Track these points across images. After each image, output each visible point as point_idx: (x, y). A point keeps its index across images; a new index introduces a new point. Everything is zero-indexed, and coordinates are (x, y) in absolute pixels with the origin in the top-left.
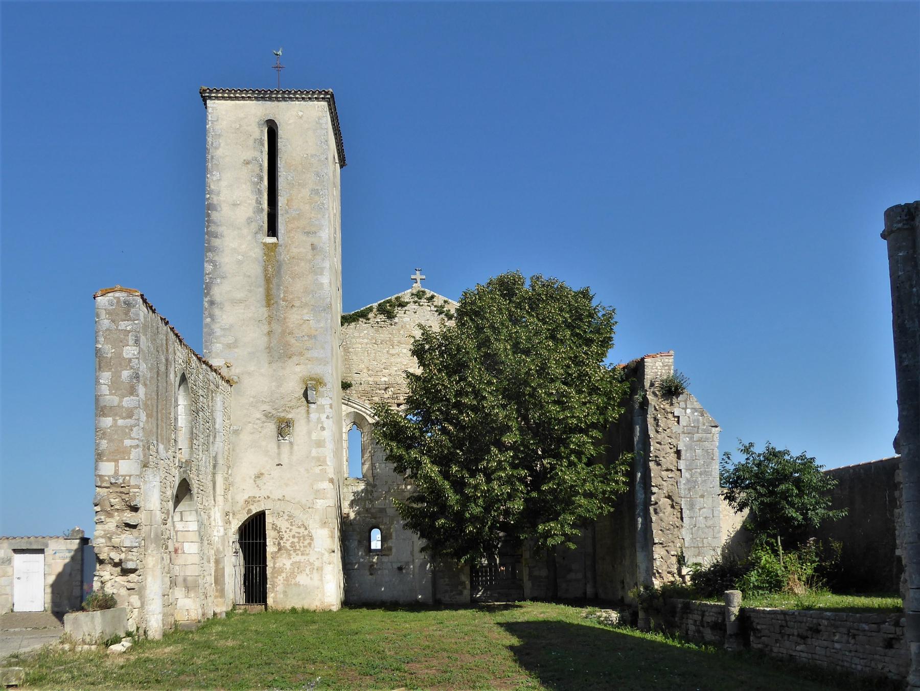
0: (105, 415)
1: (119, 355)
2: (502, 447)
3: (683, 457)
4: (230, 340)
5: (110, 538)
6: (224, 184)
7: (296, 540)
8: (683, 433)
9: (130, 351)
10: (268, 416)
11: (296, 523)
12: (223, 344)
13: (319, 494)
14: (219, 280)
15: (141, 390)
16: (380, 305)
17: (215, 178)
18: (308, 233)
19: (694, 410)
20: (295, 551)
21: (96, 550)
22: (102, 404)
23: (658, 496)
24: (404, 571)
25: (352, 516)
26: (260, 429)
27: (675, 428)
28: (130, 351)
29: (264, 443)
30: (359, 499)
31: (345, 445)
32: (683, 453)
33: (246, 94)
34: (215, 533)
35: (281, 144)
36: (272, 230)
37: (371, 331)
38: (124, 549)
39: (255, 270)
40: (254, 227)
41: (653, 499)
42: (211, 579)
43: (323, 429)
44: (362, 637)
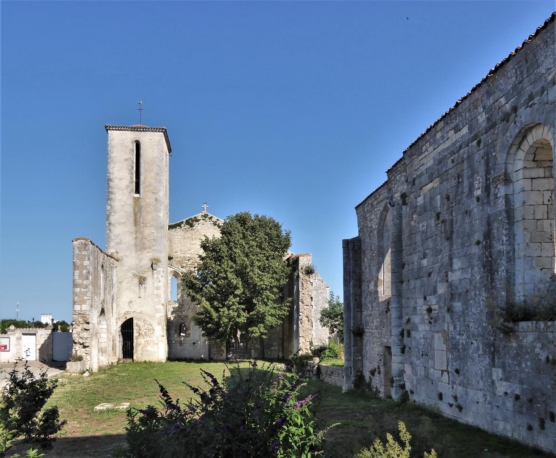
0: (77, 287)
1: (82, 264)
2: (236, 296)
3: (313, 300)
4: (118, 241)
5: (79, 334)
6: (115, 169)
7: (147, 331)
8: (314, 290)
9: (86, 263)
10: (135, 275)
11: (147, 323)
12: (115, 243)
13: (157, 311)
14: (113, 214)
15: (90, 277)
16: (187, 221)
17: (111, 167)
18: (154, 193)
19: (319, 280)
20: (146, 336)
21: (74, 339)
22: (75, 283)
23: (302, 316)
24: (196, 344)
25: (172, 319)
26: (131, 281)
27: (311, 288)
28: (86, 263)
29: (133, 288)
30: (175, 311)
31: (169, 286)
32: (313, 298)
33: (126, 128)
34: (113, 329)
35: (142, 152)
36: (138, 191)
37: (183, 233)
38: (84, 338)
39: (130, 209)
40: (129, 189)
41: (300, 318)
42: (111, 348)
43: (160, 281)
44: (174, 373)
